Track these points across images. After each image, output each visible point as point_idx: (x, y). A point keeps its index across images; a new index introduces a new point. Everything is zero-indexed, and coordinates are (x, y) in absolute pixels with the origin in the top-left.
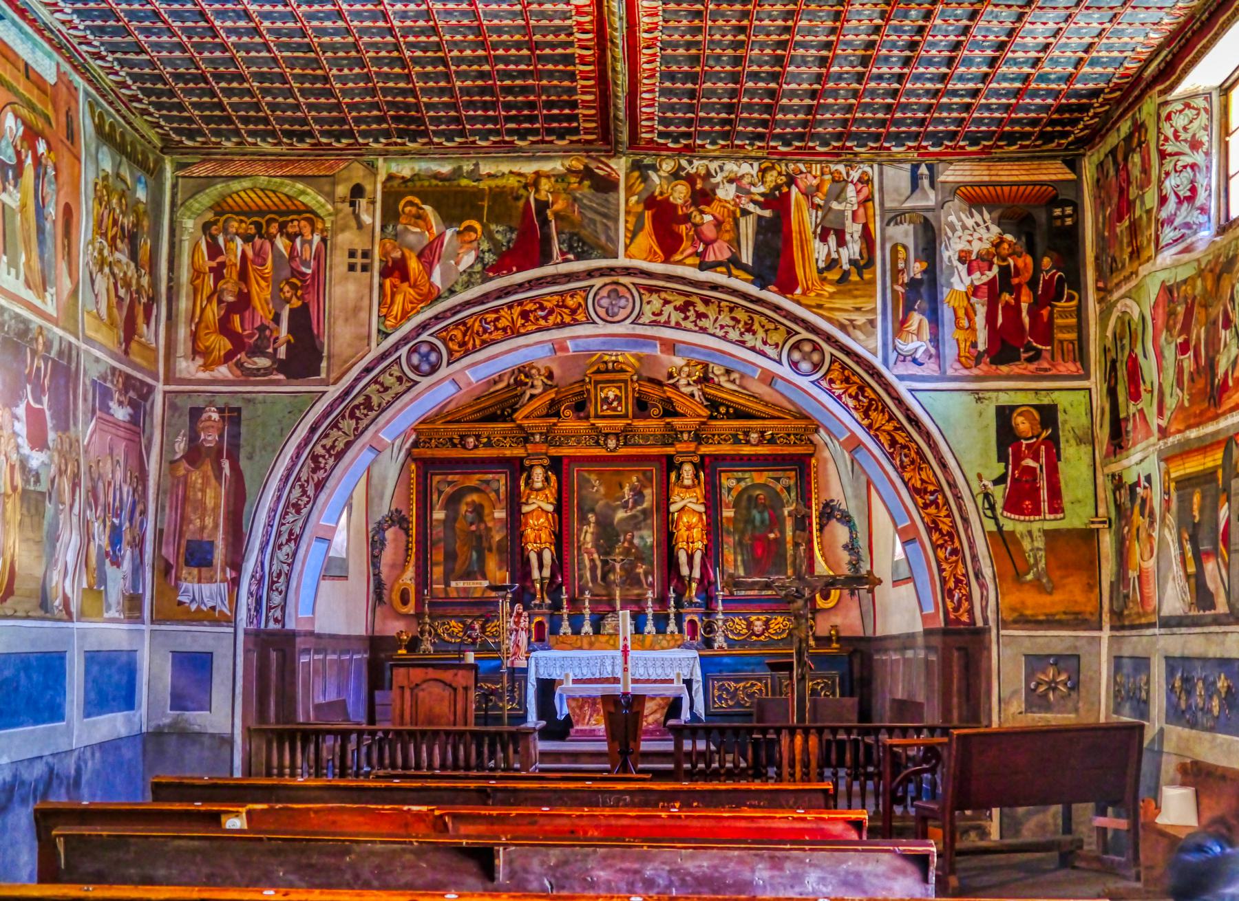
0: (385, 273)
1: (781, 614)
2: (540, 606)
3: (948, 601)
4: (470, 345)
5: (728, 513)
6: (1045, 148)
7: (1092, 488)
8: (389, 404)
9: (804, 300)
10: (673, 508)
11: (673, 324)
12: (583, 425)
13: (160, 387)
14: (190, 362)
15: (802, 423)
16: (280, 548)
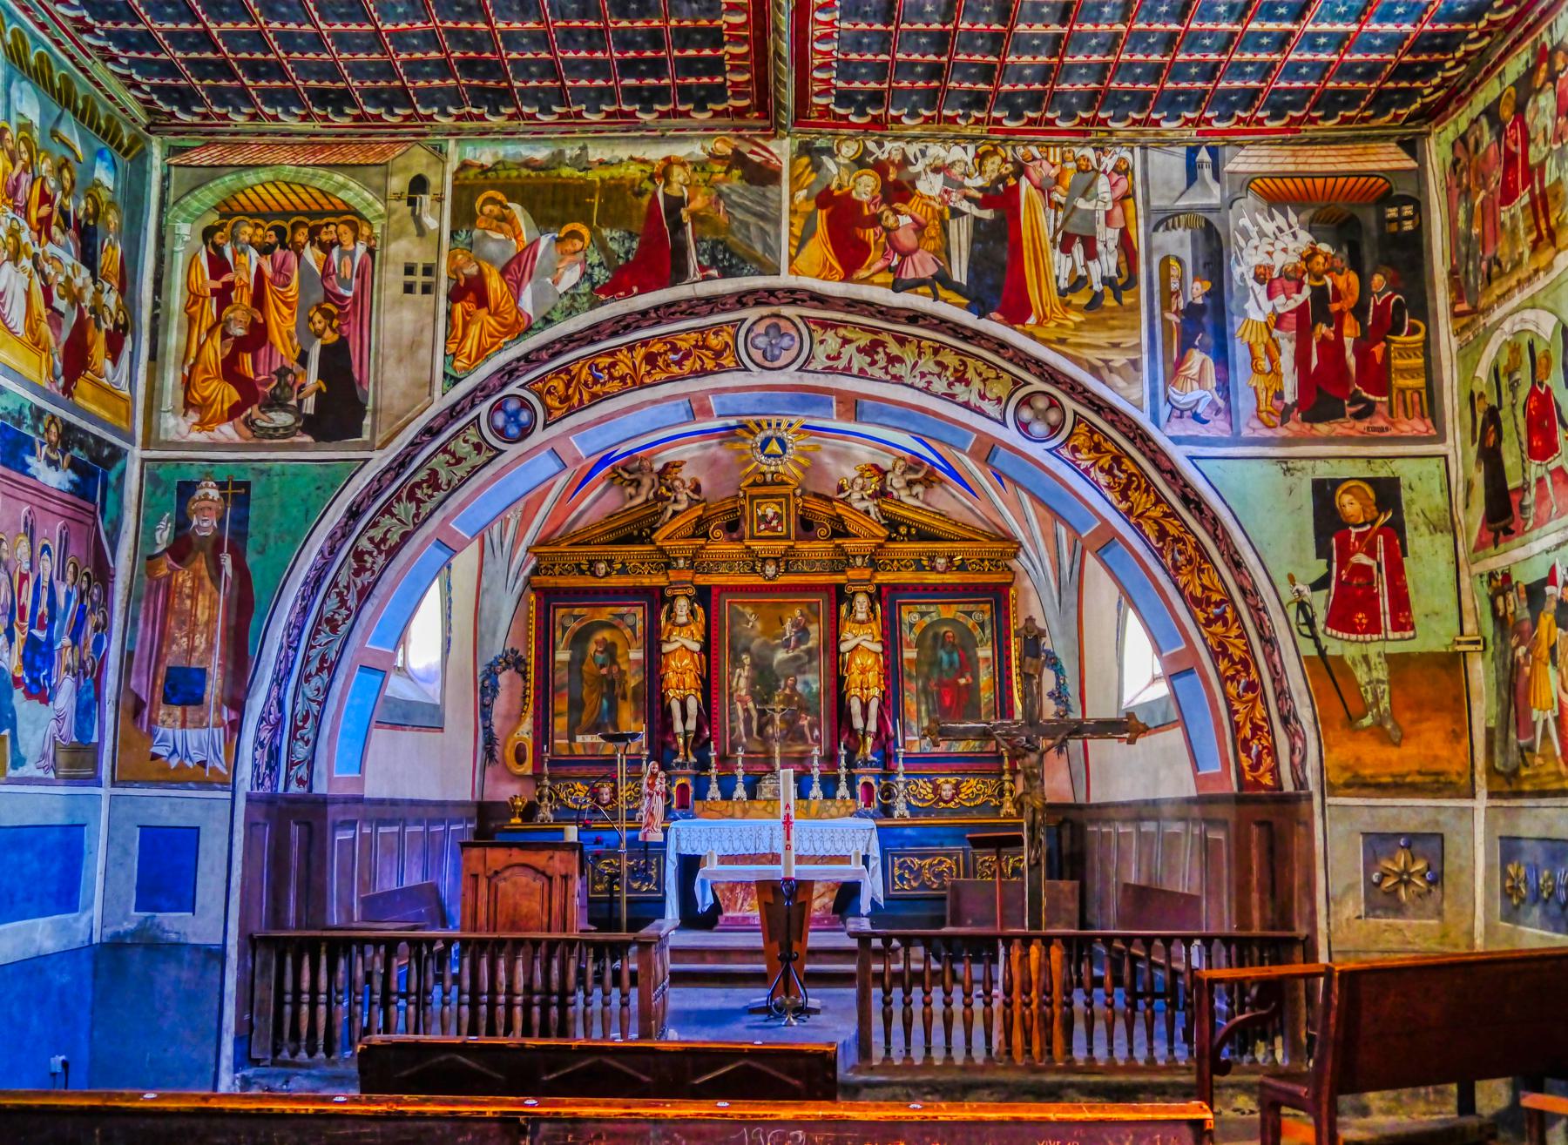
0: (455, 296)
1: (974, 775)
2: (683, 765)
3: (1243, 756)
4: (575, 401)
5: (910, 654)
6: (1374, 123)
7: (1455, 595)
8: (463, 481)
9: (1039, 333)
10: (844, 647)
11: (855, 371)
12: (737, 548)
13: (136, 453)
14: (181, 420)
15: (998, 546)
16: (307, 681)
